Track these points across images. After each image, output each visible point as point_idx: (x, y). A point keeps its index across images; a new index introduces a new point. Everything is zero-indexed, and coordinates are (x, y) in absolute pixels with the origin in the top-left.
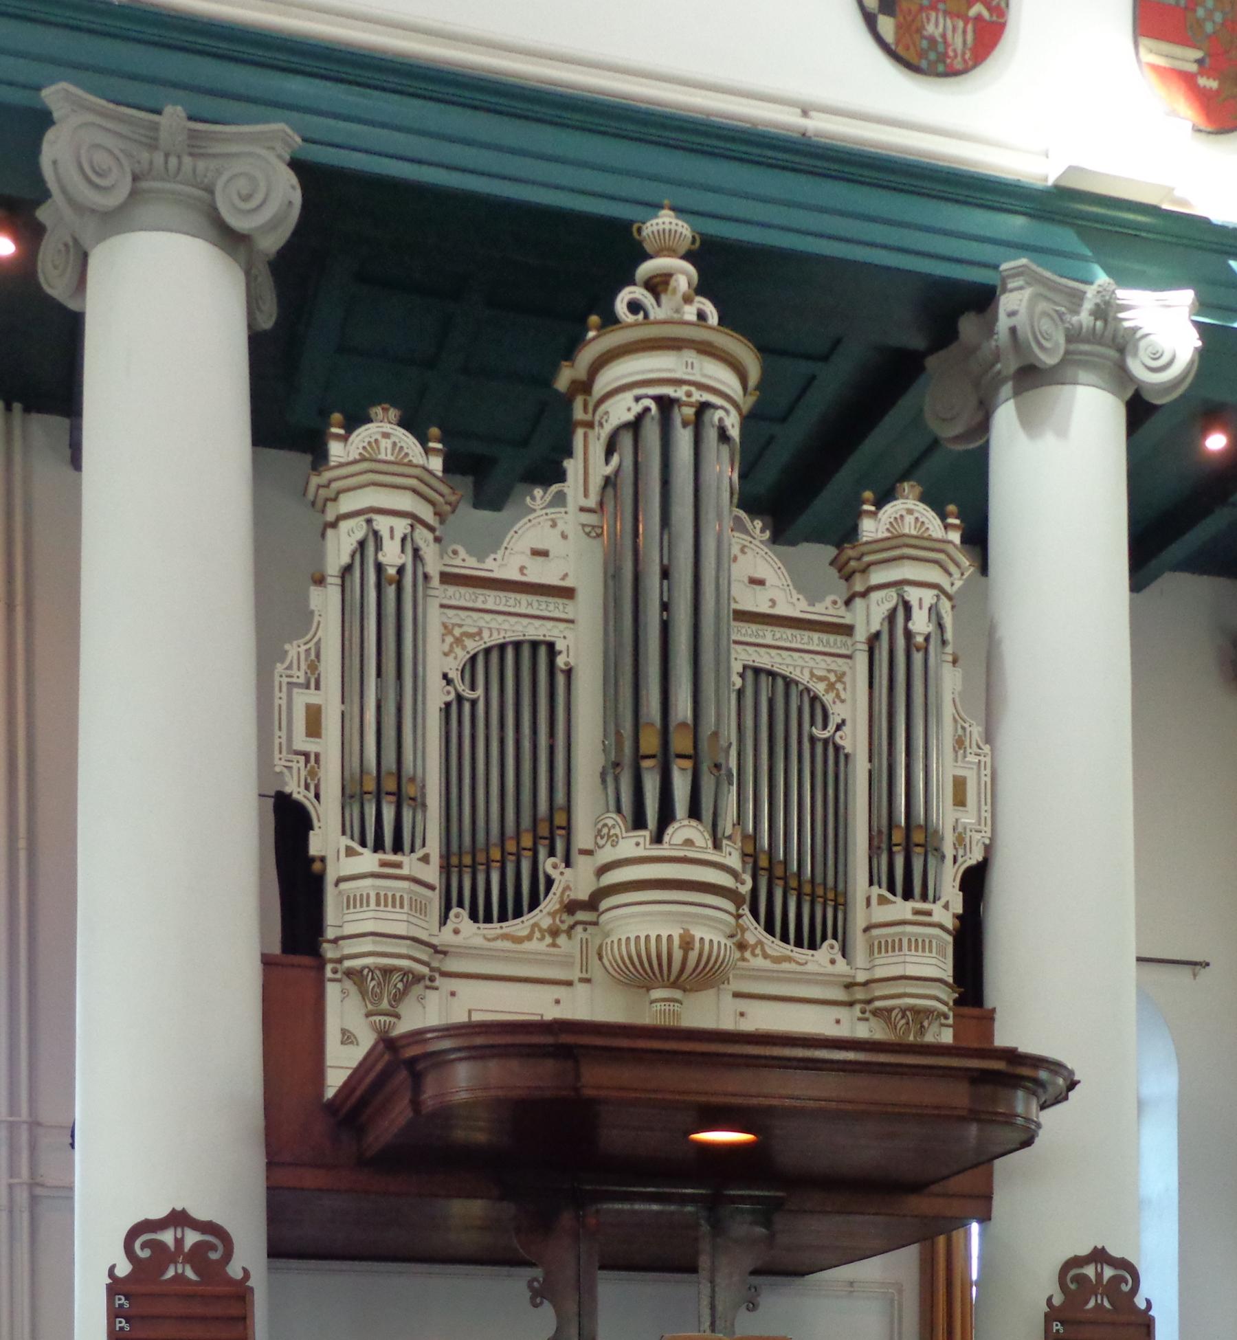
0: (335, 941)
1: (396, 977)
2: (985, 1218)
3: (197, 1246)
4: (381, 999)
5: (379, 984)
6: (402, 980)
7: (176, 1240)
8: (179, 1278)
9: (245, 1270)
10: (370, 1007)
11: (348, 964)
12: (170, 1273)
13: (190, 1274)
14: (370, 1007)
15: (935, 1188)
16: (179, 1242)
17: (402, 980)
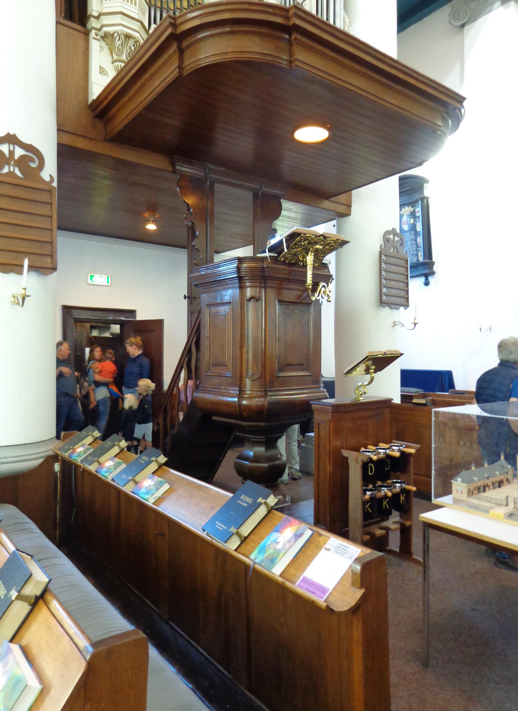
0: (97, 18)
1: (131, 42)
2: (188, 405)
3: (22, 157)
4: (122, 53)
5: (122, 44)
6: (134, 45)
7: (10, 150)
8: (11, 174)
9: (50, 176)
10: (115, 57)
11: (105, 29)
12: (6, 170)
13: (17, 172)
14: (115, 57)
15: (333, 199)
16: (12, 153)
17: (134, 45)
